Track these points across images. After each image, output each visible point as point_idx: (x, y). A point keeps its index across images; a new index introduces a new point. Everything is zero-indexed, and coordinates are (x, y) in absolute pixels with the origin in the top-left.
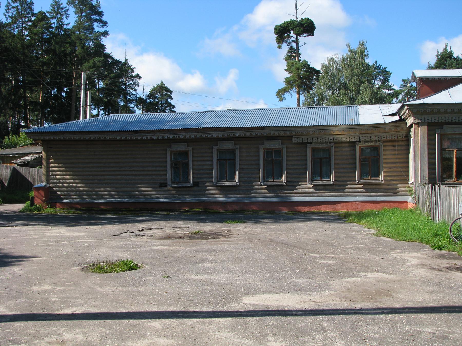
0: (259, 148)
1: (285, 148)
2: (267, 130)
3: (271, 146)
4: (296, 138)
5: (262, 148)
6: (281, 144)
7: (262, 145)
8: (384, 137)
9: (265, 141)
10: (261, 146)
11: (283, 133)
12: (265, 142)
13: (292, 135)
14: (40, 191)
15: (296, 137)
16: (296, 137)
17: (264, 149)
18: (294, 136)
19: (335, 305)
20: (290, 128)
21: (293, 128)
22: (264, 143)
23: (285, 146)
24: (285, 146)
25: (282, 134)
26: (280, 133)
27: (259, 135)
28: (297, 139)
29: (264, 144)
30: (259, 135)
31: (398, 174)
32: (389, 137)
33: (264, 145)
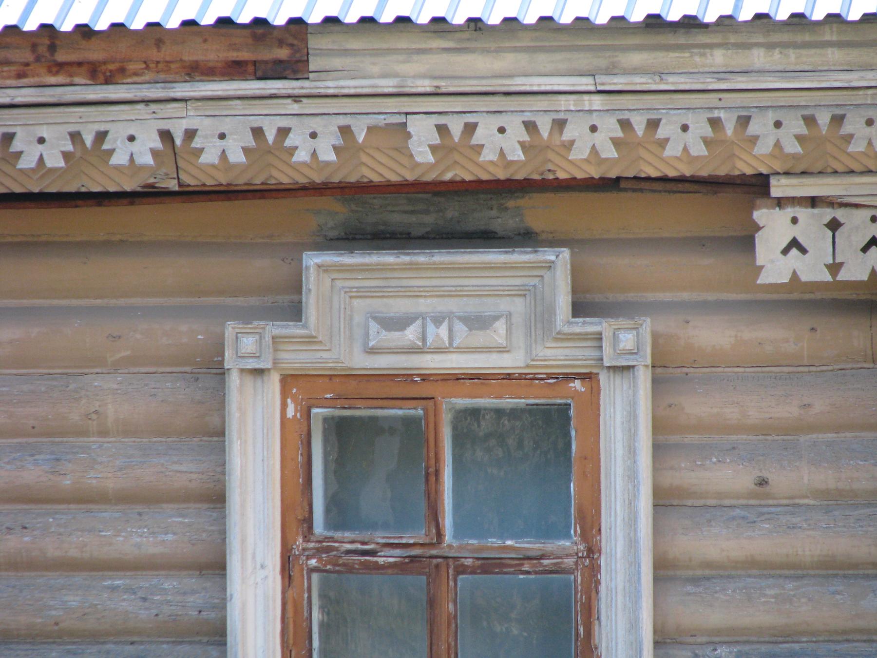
0: (222, 373)
1: (644, 378)
2: (350, 85)
3: (411, 334)
4: (803, 213)
5: (259, 372)
6: (563, 302)
7: (274, 329)
8: (795, 243)
9: (312, 260)
10: (248, 344)
11: (610, 127)
12: (312, 281)
13: (745, 166)
14: (621, 186)
15: (813, 202)
16: (813, 202)
17: (288, 381)
18: (779, 188)
19: (233, 57)
20: (718, 58)
21: (758, 58)
22: (296, 286)
23: (627, 340)
24: (627, 340)
25: (579, 153)
26: (560, 125)
27: (210, 157)
28: (834, 225)
29: (295, 312)
30: (210, 157)
31: (630, 327)
32: (795, 243)
33: (293, 329)
